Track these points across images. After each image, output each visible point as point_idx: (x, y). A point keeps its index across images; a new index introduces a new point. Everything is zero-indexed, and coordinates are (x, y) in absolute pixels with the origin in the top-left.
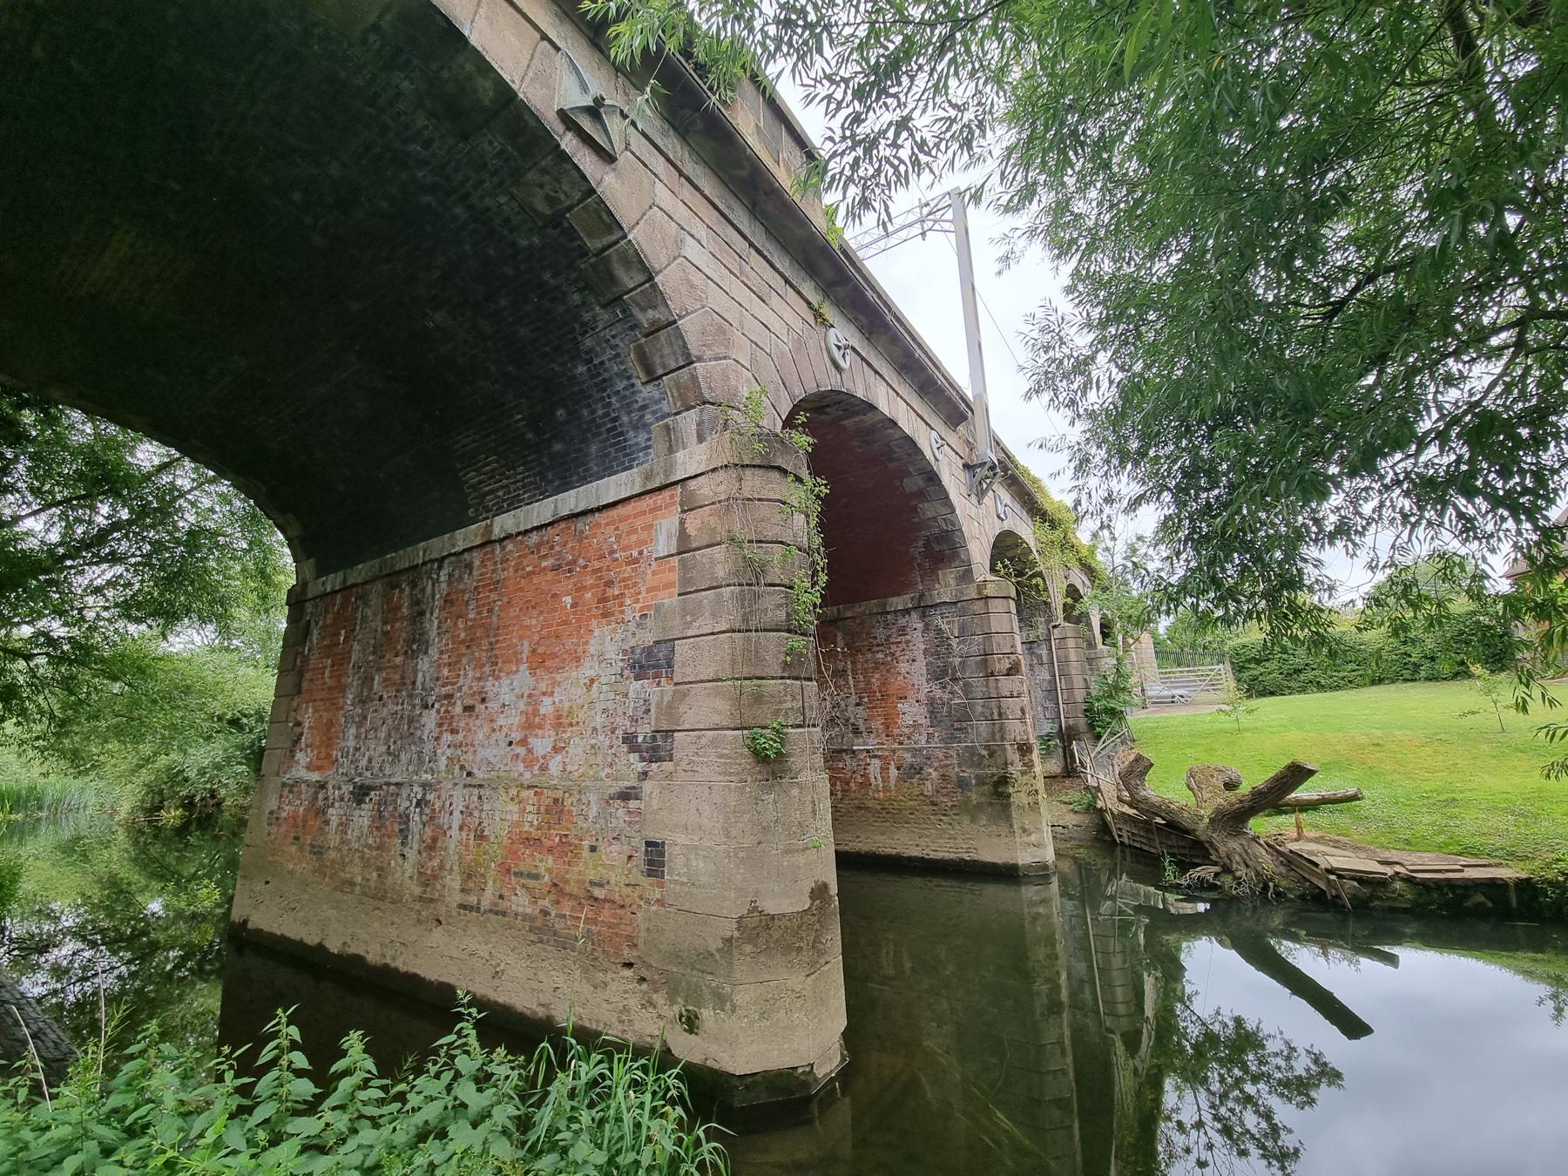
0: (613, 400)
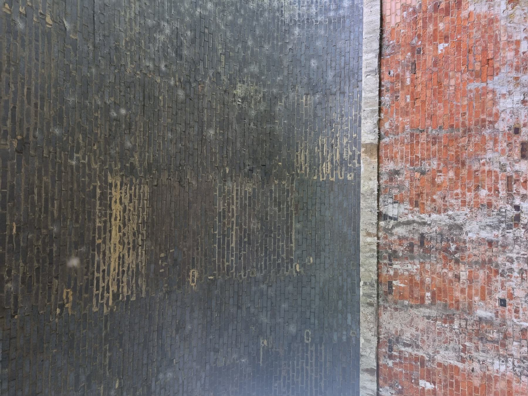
0: (319, 19)
